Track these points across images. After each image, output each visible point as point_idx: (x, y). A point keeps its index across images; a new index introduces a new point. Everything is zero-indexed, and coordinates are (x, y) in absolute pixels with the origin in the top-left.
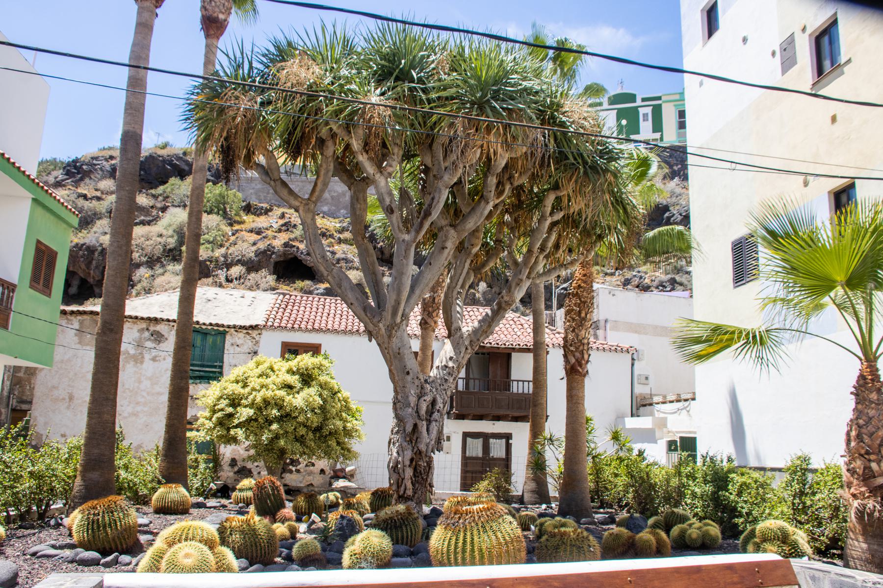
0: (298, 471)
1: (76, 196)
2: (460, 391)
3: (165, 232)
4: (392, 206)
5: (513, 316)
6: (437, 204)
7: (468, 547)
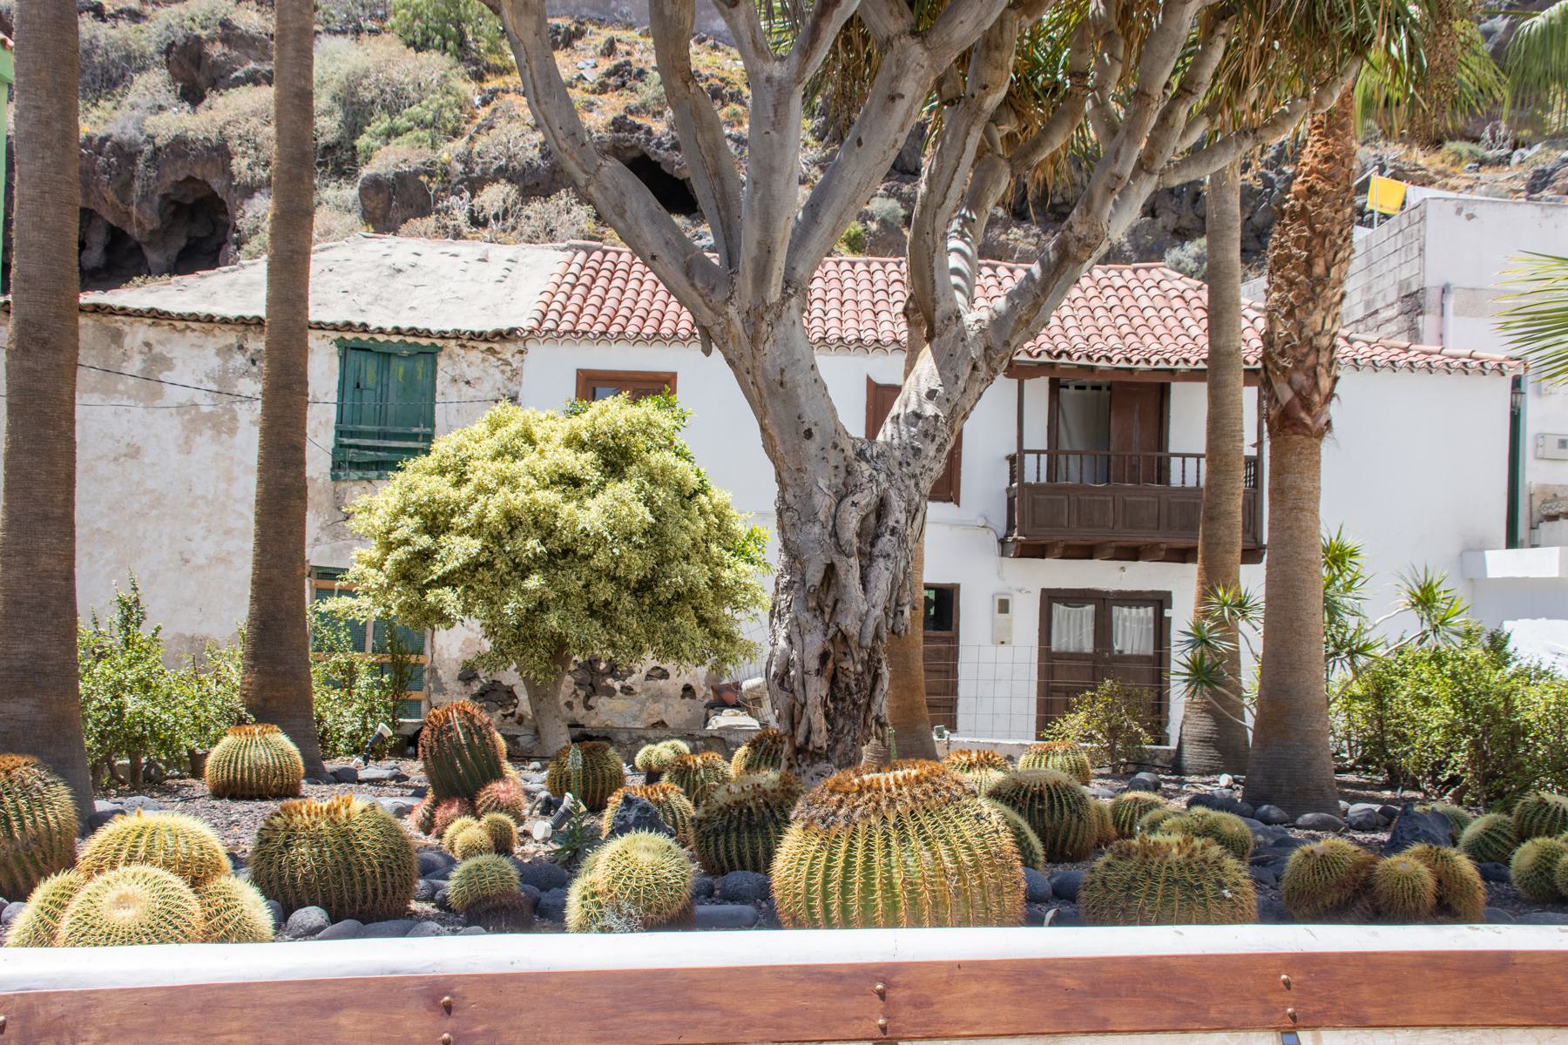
0: (628, 691)
2: (1029, 485)
5: (1181, 286)
7: (857, 877)
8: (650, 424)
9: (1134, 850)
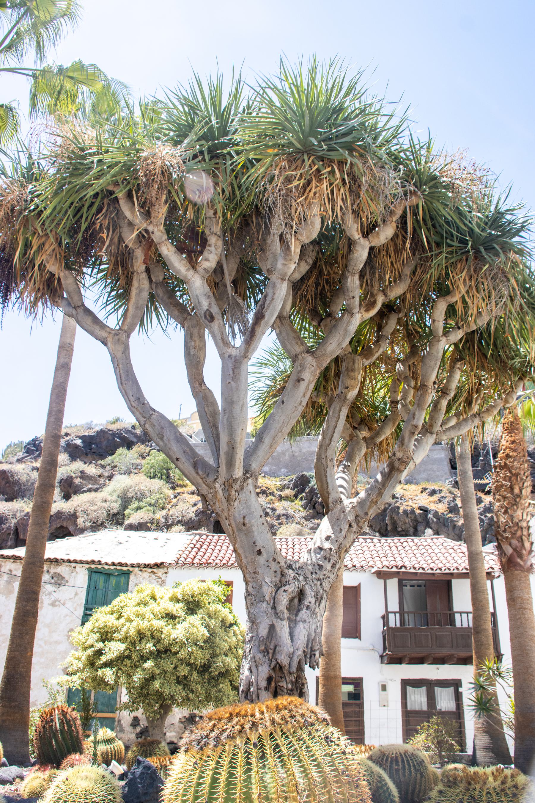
1: (30, 469)
2: (392, 628)
3: (109, 498)
4: (212, 311)
5: (452, 545)
6: (271, 302)
8: (209, 590)
9: (459, 779)
